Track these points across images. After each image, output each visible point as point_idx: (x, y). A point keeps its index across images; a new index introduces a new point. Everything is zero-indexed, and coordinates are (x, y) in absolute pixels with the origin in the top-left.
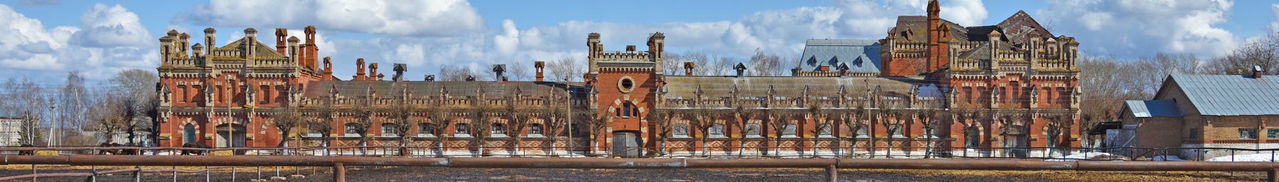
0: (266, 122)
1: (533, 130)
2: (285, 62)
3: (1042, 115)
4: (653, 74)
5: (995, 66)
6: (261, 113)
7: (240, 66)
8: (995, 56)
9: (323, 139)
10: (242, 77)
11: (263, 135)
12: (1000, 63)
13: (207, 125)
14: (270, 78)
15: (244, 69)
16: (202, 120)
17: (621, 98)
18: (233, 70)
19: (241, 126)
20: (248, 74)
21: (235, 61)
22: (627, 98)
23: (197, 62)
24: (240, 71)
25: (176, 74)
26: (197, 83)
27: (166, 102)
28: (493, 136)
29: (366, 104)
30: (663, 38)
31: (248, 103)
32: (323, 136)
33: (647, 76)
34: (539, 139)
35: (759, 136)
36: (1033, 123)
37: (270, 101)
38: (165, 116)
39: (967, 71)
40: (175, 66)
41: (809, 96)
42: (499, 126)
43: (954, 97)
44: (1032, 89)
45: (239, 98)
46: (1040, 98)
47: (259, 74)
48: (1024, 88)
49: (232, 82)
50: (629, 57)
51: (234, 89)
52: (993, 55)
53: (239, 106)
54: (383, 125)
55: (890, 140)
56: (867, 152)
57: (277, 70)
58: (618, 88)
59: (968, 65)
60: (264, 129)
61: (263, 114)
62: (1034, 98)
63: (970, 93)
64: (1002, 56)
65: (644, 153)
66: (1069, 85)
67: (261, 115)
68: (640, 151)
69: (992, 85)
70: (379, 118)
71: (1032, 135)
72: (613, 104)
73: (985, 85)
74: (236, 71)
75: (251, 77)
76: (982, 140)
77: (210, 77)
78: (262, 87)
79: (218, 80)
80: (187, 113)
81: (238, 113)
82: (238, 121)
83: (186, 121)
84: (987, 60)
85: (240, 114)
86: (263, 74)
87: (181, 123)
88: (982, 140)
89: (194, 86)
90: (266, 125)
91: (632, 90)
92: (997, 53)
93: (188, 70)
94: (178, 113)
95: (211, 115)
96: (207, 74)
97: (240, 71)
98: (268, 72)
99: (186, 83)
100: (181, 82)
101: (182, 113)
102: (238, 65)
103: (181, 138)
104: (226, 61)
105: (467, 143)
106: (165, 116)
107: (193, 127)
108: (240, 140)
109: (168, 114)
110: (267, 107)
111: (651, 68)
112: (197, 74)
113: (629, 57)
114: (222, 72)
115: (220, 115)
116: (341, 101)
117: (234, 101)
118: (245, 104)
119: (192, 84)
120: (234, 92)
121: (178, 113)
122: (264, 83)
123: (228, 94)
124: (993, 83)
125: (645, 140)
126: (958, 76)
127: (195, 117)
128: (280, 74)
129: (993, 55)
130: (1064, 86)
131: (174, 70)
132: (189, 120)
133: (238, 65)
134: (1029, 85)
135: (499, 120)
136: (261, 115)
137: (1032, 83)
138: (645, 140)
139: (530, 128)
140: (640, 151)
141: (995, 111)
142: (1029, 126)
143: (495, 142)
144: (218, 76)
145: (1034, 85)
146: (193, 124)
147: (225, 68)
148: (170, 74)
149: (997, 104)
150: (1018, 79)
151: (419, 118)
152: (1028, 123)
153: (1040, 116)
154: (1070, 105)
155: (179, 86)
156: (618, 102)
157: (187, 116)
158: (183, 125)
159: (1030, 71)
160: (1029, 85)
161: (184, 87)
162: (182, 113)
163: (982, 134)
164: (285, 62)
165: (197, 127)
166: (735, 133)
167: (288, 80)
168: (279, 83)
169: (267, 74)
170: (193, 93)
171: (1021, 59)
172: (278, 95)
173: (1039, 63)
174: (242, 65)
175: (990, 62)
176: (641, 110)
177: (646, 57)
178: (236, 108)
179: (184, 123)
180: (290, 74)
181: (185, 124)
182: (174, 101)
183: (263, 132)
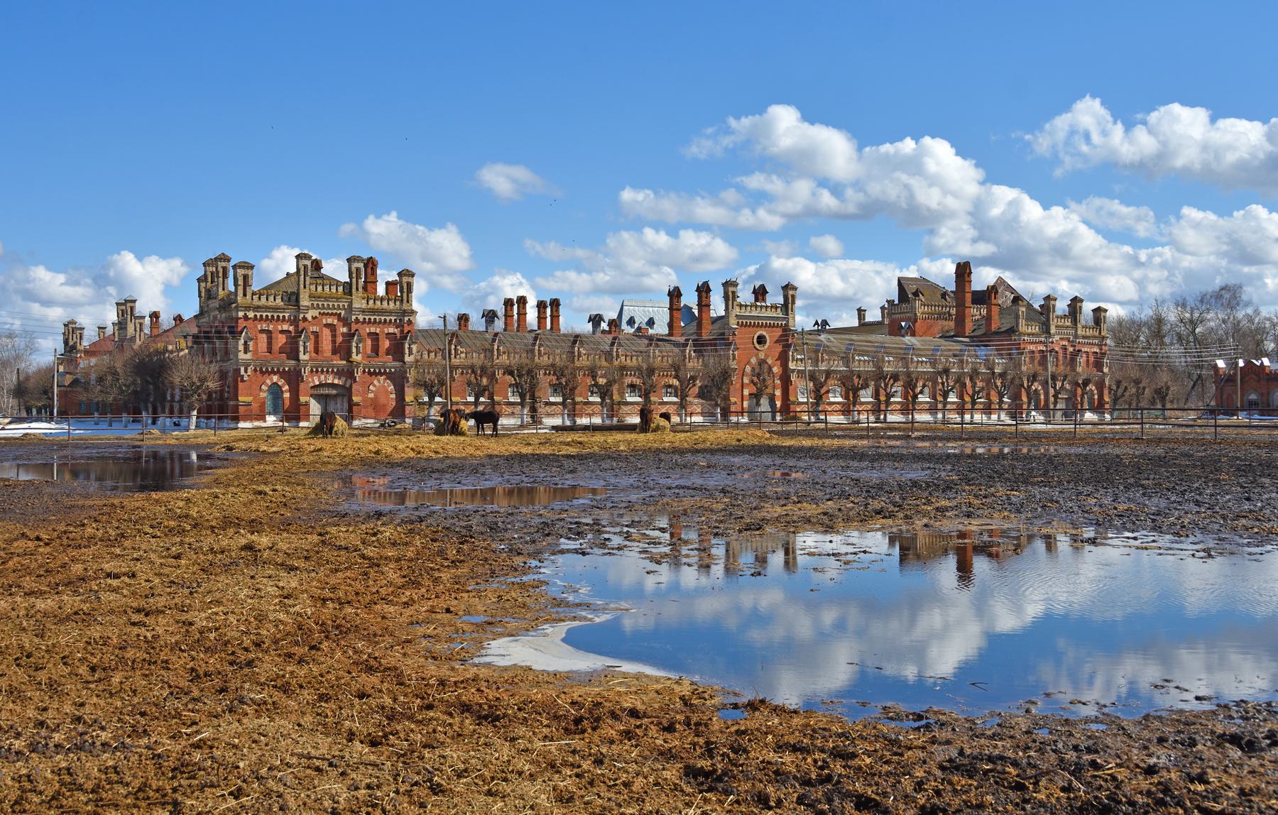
0: (376, 382)
1: (667, 392)
2: (398, 303)
3: (367, 370)
4: (786, 329)
5: (305, 301)
6: (369, 370)
7: (344, 305)
8: (305, 287)
9: (563, 404)
10: (345, 322)
11: (371, 399)
12: (1056, 327)
13: (302, 386)
14: (380, 322)
15: (350, 309)
16: (294, 378)
17: (757, 355)
18: (334, 311)
19: (343, 386)
20: (354, 317)
21: (338, 299)
22: (762, 356)
23: (285, 298)
24: (343, 312)
25: (258, 314)
26: (285, 327)
27: (246, 352)
28: (629, 399)
29: (533, 359)
30: (737, 285)
31: (354, 355)
32: (564, 400)
33: (778, 332)
34: (674, 403)
35: (871, 400)
36: (355, 381)
37: (380, 354)
38: (246, 372)
39: (267, 308)
40: (256, 302)
41: (459, 347)
42: (633, 387)
43: (357, 347)
44: (354, 334)
45: (343, 350)
46: (365, 347)
47: (367, 318)
48: (343, 334)
49: (331, 327)
50: (764, 310)
51: (334, 336)
52: (302, 286)
53: (341, 360)
54: (511, 385)
55: (945, 403)
56: (957, 416)
57: (390, 313)
58: (755, 347)
59: (267, 300)
60: (373, 391)
61: (372, 370)
62: (305, 347)
63: (377, 340)
64: (313, 287)
65: (778, 418)
66: (297, 326)
67: (370, 373)
68: (774, 418)
69: (405, 332)
70: (547, 376)
71: (354, 398)
72: (748, 363)
73: (291, 328)
74: (338, 312)
75: (357, 321)
76: (1042, 403)
77: (305, 319)
78: (370, 334)
79: (314, 325)
80: (273, 369)
81: (340, 369)
82: (339, 379)
83: (271, 380)
84: (293, 293)
85: (343, 370)
86: (372, 318)
87: (264, 383)
88: (1042, 403)
89: (282, 332)
90: (375, 386)
91: (766, 347)
92: (308, 283)
93: (276, 309)
94: (261, 369)
95: (306, 373)
96: (302, 316)
97: (343, 312)
98: (378, 315)
99: (271, 327)
100: (265, 326)
101: (267, 369)
102: (341, 304)
103: (264, 403)
104: (326, 299)
105: (899, 407)
106: (246, 372)
107: (280, 387)
108: (339, 406)
109: (249, 370)
110: (377, 362)
111: (784, 323)
112: (287, 315)
113: (764, 310)
114: (320, 313)
115: (317, 371)
116: (463, 355)
117: (334, 352)
118: (351, 357)
119: (280, 328)
120: (334, 342)
121: (261, 369)
122: (373, 330)
123: (326, 345)
124: (301, 325)
125: (778, 404)
126: (251, 314)
127: (282, 374)
128: (393, 318)
129: (302, 286)
130: (1098, 351)
131: (257, 308)
132: (275, 378)
133: (341, 304)
134: (350, 330)
135: (634, 380)
136: (370, 373)
137: (354, 327)
138: (778, 404)
139: (664, 391)
140: (774, 418)
141: (358, 364)
142: (351, 386)
143: (630, 407)
144: (314, 318)
145: (357, 330)
146: (280, 383)
147: (324, 308)
148: (251, 314)
149: (360, 355)
150: (335, 322)
151: (551, 377)
152: (349, 381)
153: (364, 371)
154: (404, 357)
155: (262, 331)
156: (753, 360)
157: (273, 372)
158: (267, 385)
159: (1076, 336)
160: (350, 330)
161: (269, 332)
162: (267, 369)
163: (1042, 397)
164: (398, 303)
165: (286, 387)
166: (242, 395)
167: (403, 326)
168: (391, 330)
169: (378, 318)
170: (281, 340)
171: (1069, 324)
172: (284, 341)
173: (363, 298)
174: (346, 304)
175: (297, 295)
176: (775, 369)
177: (779, 310)
178: (340, 362)
179: (269, 382)
180: (406, 319)
181: (270, 384)
182: (255, 352)
183: (371, 395)
